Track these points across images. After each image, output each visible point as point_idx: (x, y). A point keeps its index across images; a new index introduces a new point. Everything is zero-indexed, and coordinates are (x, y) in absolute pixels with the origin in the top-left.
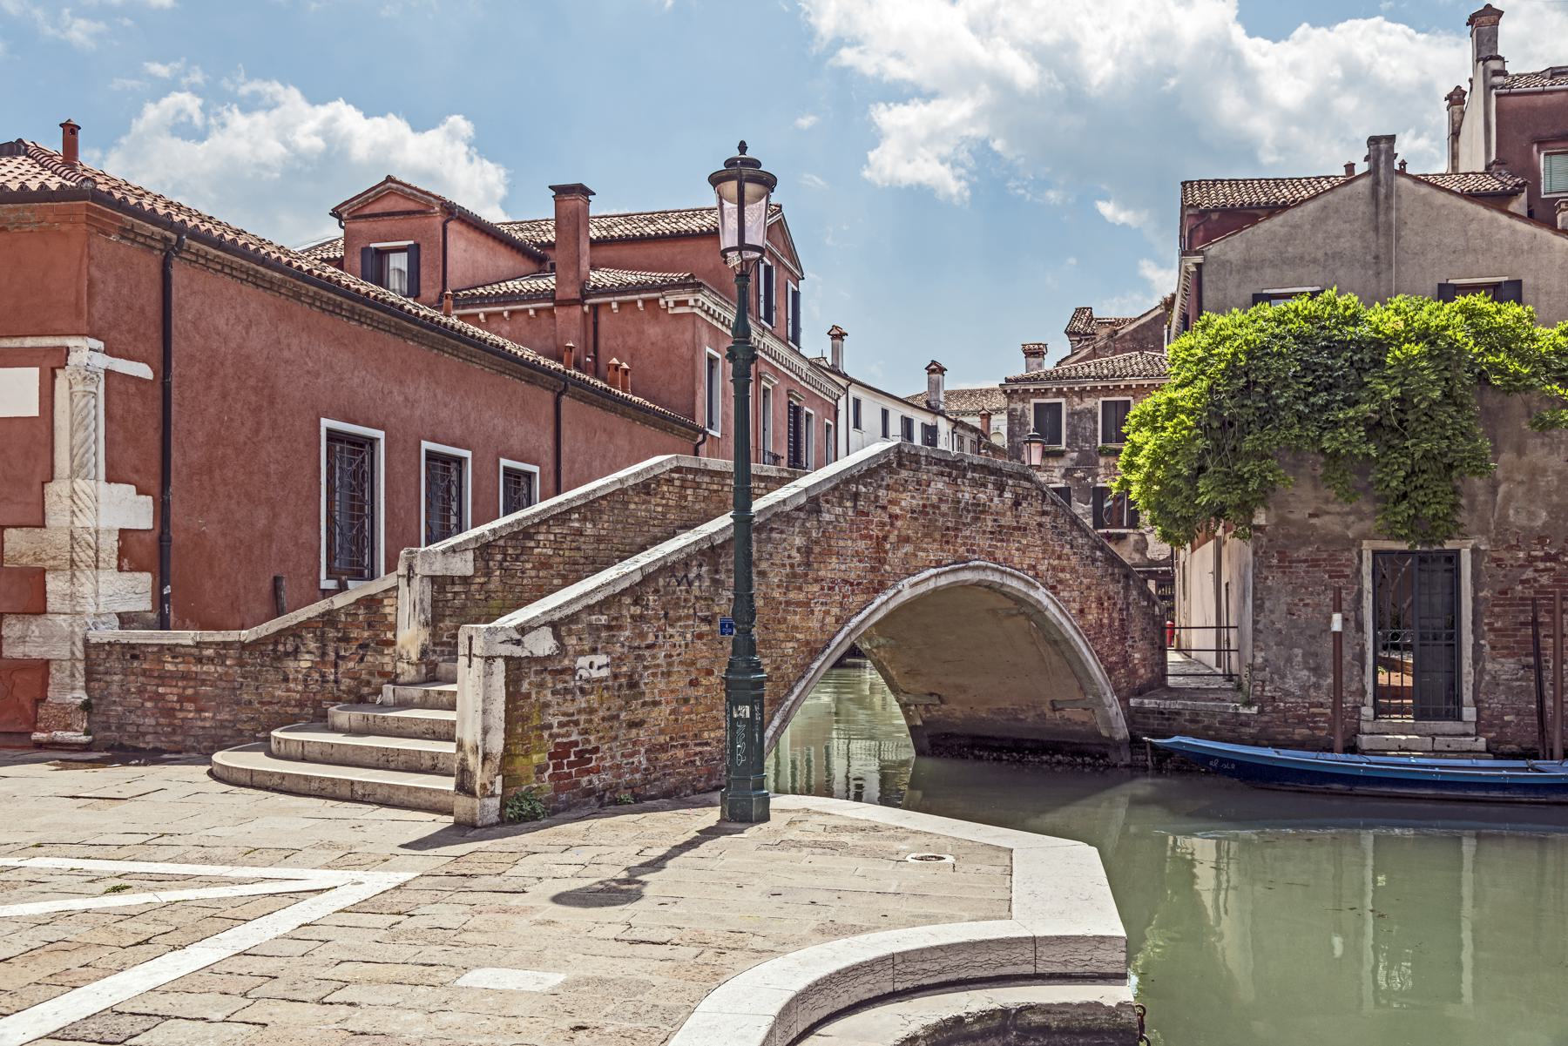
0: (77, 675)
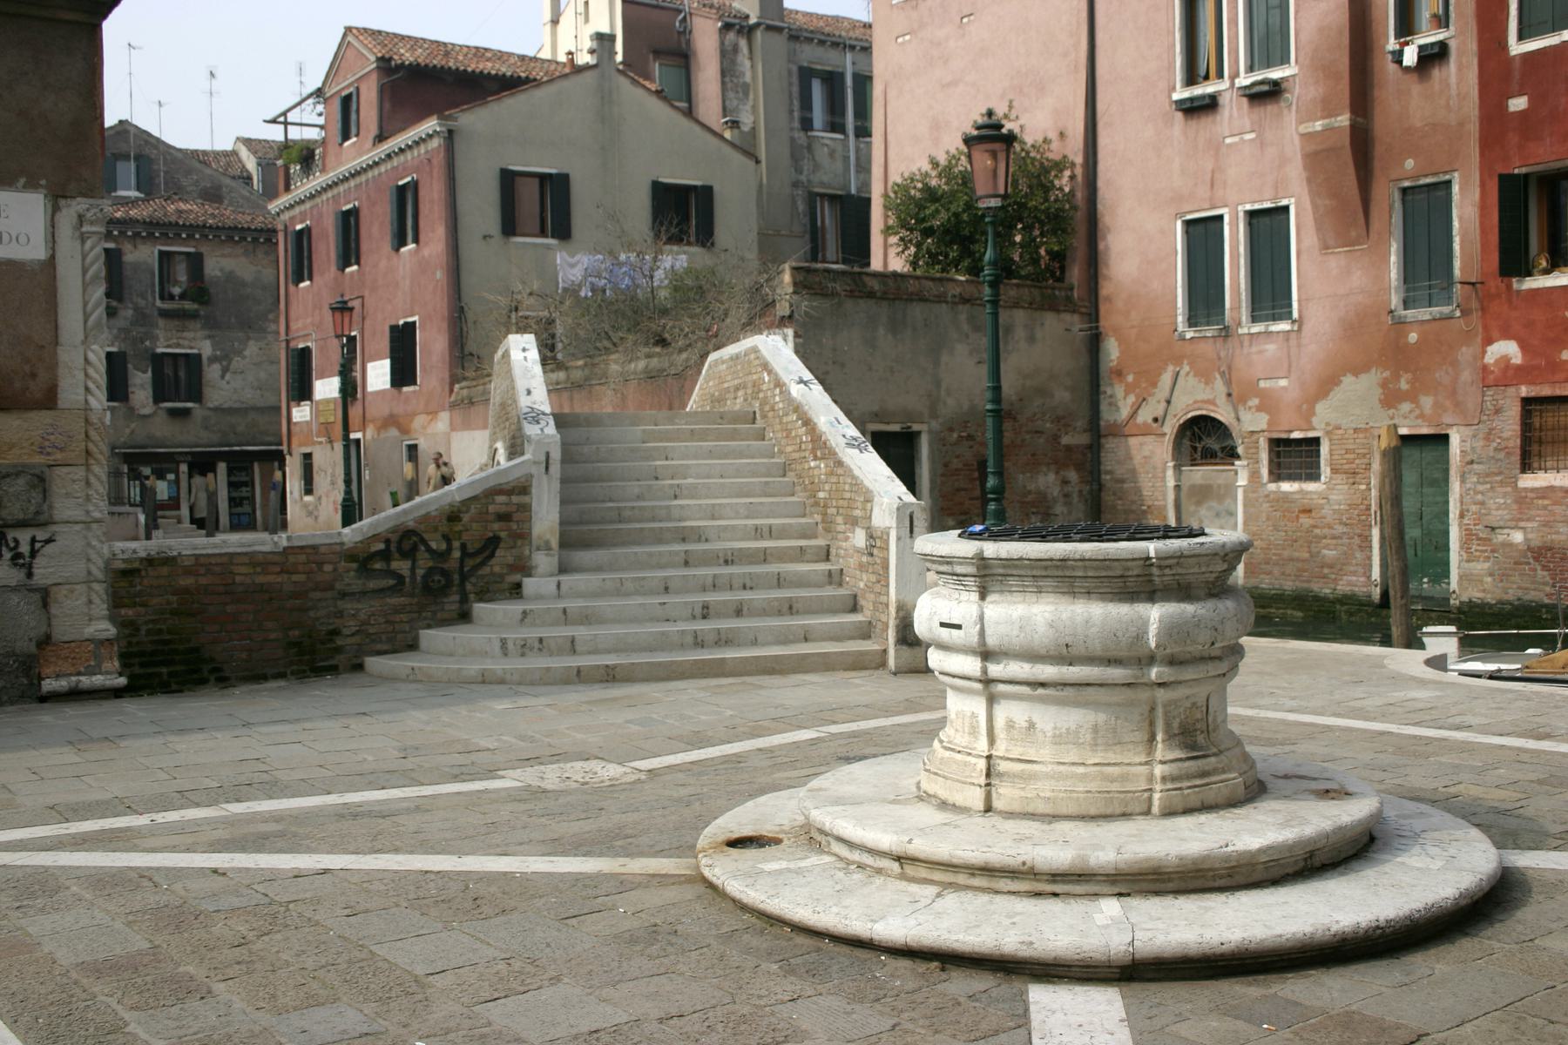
0: (97, 600)
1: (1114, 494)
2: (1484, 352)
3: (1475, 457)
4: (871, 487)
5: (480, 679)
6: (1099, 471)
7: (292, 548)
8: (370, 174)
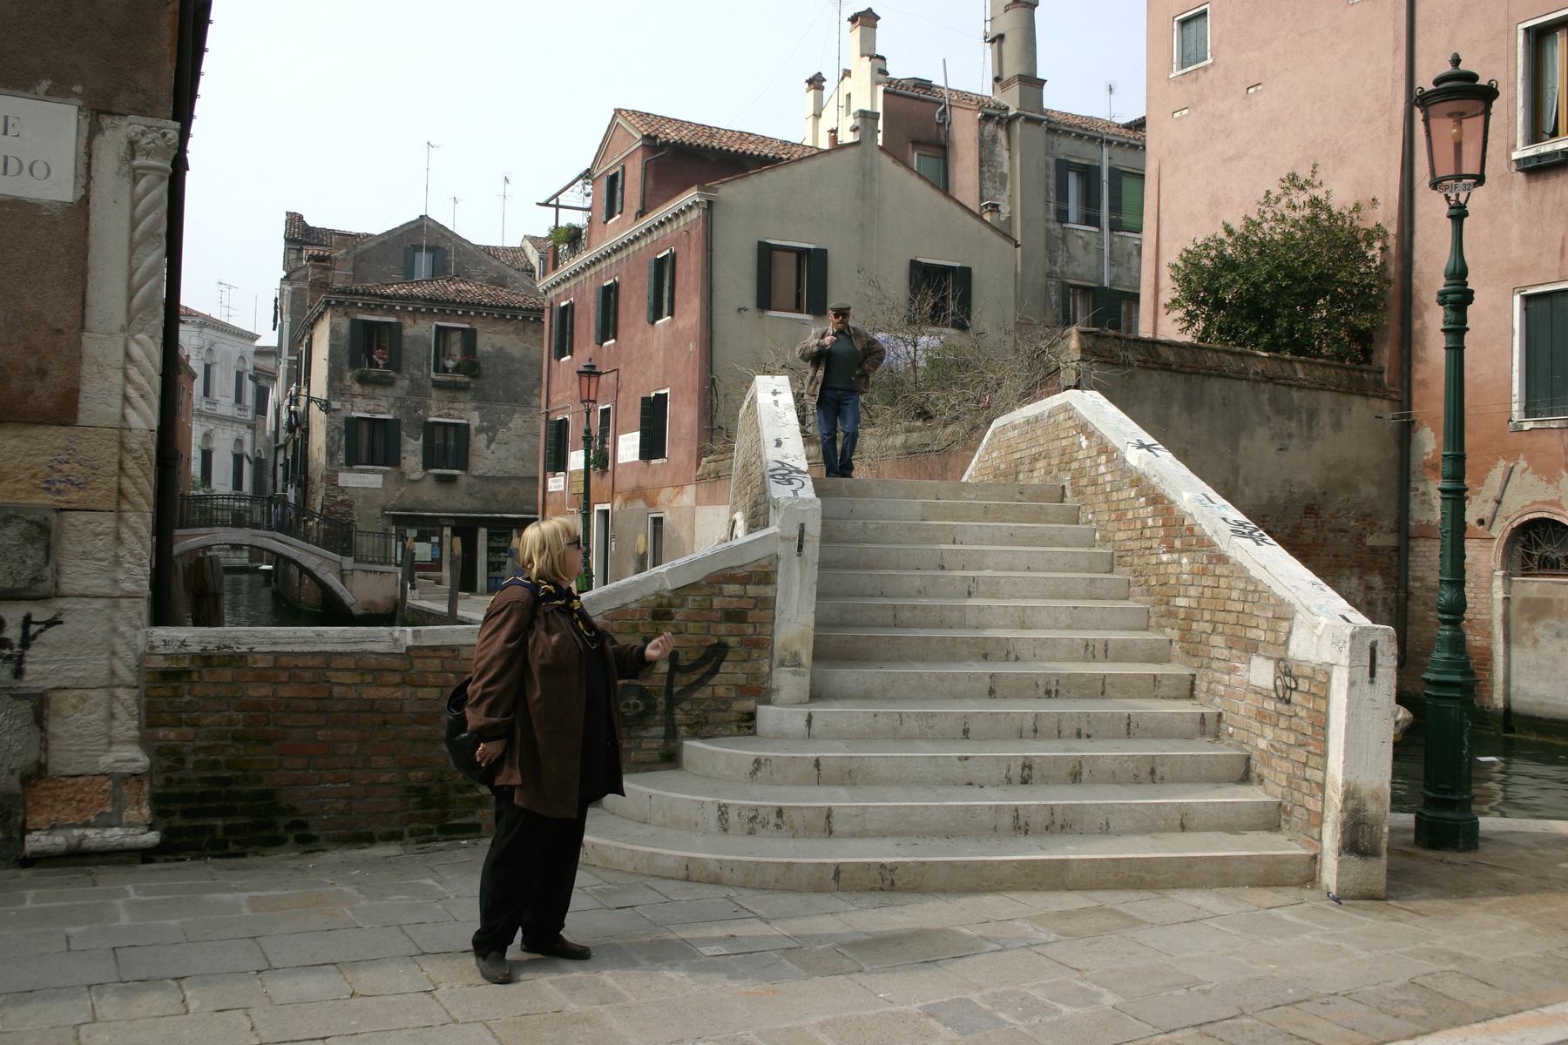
1: (1425, 604)
4: (1289, 597)
5: (682, 873)
6: (1407, 576)
7: (418, 648)
8: (631, 249)
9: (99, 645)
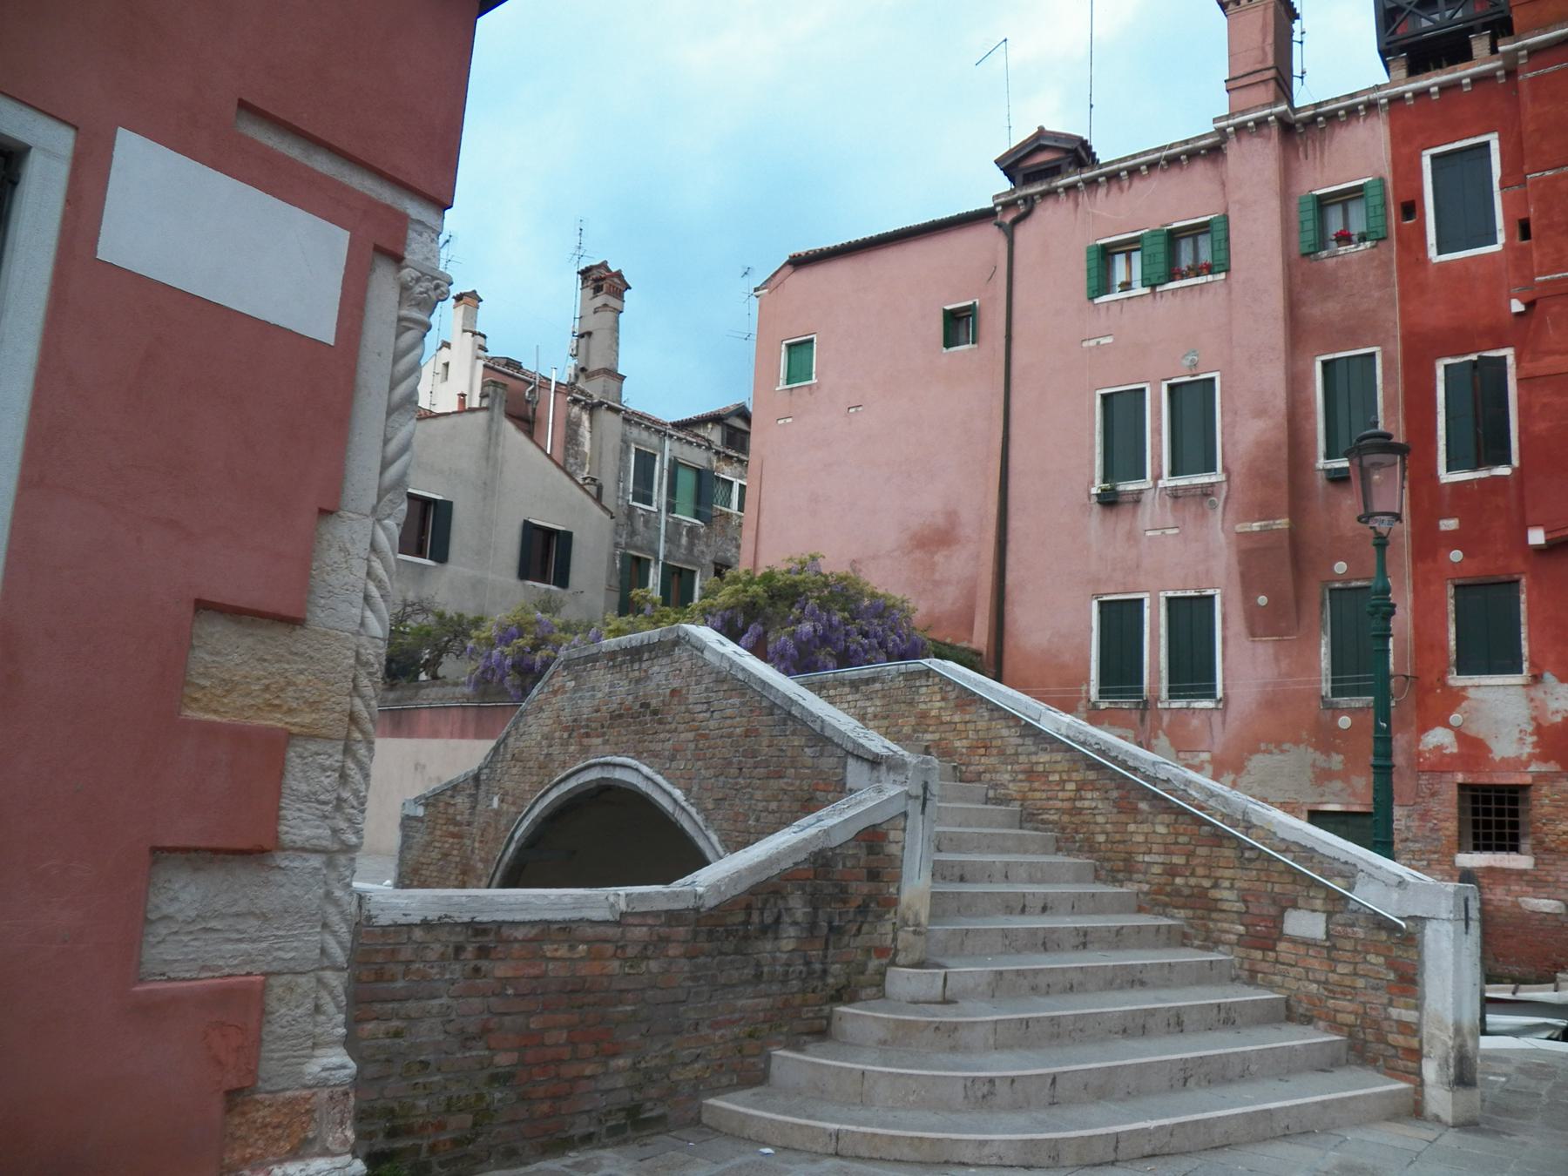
0: (330, 1008)
2: (1418, 741)
3: (1410, 836)
9: (314, 915)
